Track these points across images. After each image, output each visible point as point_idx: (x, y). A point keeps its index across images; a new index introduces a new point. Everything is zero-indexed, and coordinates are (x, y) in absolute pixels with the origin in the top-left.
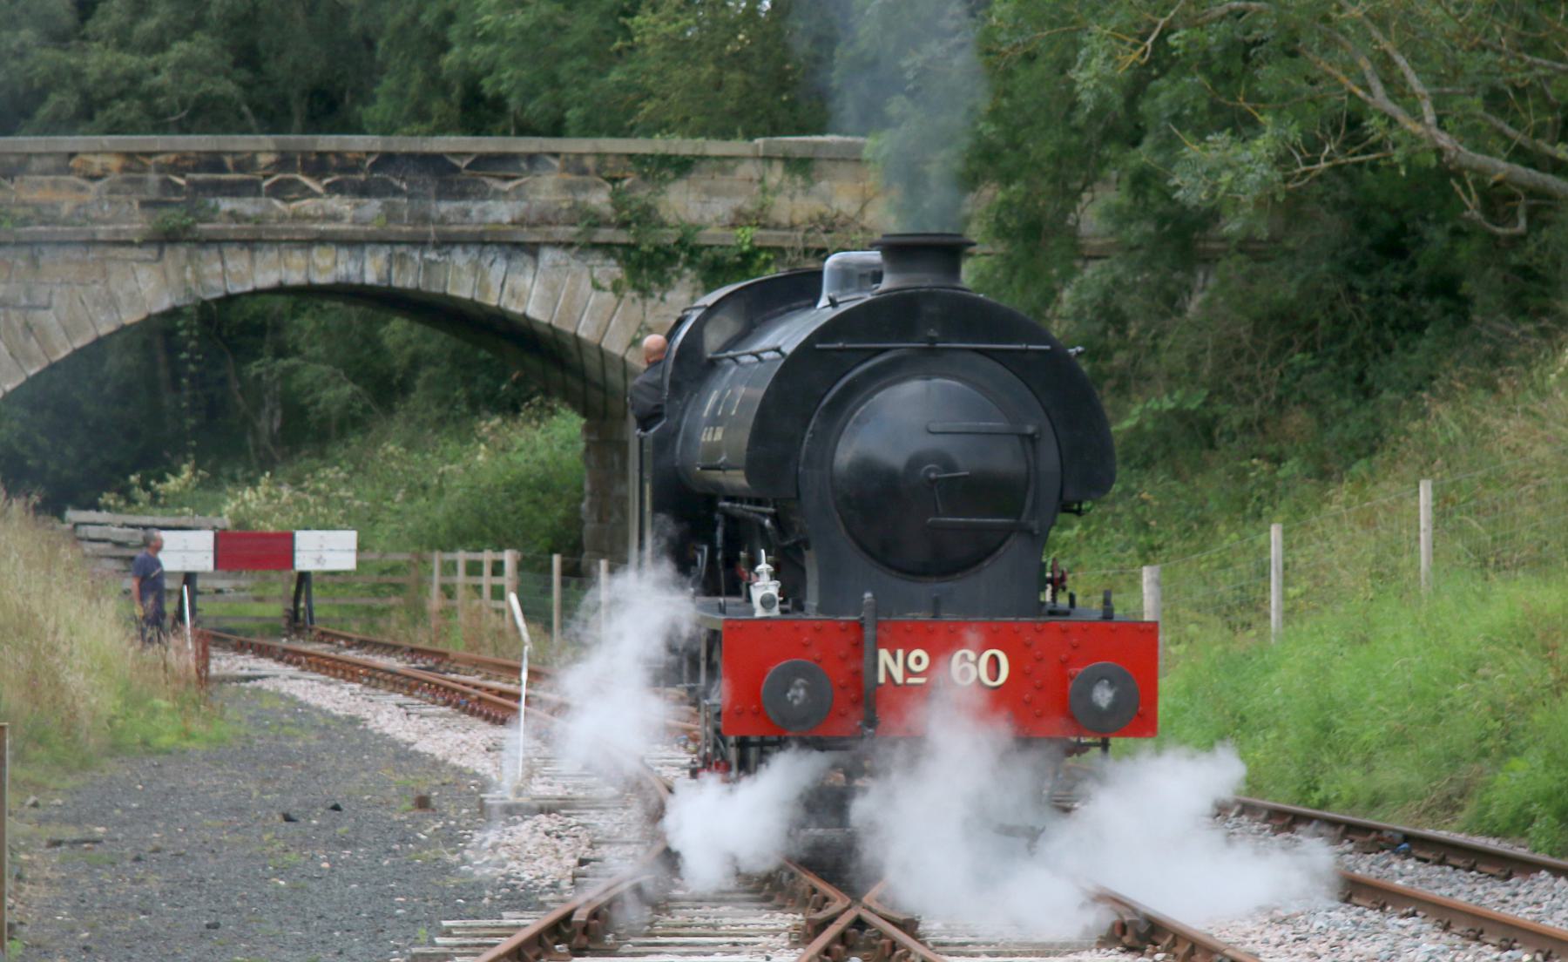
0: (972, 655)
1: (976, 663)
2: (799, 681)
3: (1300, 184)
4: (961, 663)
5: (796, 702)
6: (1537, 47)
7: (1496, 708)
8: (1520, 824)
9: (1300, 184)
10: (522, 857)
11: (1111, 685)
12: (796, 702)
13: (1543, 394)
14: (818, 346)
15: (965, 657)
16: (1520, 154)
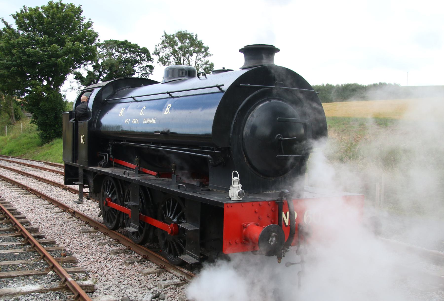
5: (272, 243)
12: (272, 243)
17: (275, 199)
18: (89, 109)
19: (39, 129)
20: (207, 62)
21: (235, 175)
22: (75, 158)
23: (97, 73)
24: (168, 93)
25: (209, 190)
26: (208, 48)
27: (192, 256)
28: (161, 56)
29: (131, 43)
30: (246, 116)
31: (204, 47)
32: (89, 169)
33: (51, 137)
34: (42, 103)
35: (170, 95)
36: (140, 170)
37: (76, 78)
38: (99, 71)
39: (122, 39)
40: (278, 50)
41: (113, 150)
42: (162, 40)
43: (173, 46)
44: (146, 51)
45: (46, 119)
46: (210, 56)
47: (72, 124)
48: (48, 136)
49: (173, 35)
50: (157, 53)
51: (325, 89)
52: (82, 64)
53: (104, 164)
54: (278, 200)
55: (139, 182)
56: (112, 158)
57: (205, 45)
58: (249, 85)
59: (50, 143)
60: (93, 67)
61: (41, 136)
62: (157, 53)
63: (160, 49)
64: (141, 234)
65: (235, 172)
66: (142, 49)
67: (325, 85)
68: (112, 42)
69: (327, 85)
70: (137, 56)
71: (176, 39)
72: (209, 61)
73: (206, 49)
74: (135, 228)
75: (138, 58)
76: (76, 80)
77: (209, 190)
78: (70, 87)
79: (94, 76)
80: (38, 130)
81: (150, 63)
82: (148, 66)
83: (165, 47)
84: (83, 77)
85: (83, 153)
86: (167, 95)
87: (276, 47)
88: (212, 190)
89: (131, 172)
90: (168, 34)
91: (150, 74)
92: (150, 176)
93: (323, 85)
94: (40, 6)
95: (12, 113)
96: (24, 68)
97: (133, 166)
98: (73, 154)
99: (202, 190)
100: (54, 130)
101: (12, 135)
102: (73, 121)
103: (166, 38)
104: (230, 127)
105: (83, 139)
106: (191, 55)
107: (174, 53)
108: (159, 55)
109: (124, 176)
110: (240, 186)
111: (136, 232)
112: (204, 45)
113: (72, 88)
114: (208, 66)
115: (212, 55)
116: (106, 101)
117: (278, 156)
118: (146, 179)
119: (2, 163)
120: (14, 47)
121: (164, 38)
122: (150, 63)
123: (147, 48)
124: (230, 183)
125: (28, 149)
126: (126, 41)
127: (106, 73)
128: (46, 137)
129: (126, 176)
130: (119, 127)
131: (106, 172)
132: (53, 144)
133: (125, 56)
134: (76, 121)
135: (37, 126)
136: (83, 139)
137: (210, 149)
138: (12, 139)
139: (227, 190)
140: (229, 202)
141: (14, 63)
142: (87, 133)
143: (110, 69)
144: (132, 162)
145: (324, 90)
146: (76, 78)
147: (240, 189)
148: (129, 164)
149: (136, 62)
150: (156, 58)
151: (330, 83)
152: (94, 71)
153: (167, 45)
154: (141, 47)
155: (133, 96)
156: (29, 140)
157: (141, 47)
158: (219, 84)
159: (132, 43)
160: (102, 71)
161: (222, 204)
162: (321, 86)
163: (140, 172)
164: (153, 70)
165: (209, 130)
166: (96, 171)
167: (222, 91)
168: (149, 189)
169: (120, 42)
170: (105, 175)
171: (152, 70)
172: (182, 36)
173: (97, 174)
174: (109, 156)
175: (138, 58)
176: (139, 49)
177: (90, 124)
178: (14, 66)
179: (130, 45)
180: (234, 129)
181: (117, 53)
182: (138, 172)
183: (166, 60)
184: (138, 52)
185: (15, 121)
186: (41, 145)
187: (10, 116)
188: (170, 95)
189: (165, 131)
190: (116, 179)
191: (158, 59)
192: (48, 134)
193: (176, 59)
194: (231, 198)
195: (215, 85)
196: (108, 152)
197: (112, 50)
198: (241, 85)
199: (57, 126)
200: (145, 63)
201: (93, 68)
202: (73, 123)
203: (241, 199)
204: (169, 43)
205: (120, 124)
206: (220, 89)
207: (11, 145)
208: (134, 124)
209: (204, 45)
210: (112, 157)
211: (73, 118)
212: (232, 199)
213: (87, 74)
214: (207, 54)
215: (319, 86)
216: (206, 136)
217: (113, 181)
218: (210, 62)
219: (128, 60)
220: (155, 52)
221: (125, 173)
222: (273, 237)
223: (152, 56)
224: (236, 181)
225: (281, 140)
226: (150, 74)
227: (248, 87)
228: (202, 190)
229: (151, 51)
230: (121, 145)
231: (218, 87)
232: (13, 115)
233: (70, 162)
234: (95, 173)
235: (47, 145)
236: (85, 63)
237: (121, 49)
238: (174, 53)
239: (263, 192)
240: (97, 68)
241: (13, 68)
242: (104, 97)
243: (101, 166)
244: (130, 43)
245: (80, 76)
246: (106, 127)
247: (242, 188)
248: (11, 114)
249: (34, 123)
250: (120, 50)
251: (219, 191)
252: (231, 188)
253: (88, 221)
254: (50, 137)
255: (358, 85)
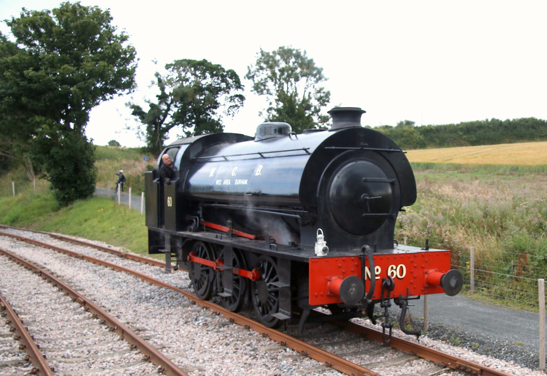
0: (394, 267)
1: (396, 270)
2: (353, 285)
3: (157, 142)
4: (391, 270)
5: (352, 293)
6: (4, 141)
7: (3, 211)
8: (6, 223)
9: (157, 142)
10: (88, 345)
11: (455, 278)
12: (352, 293)
13: (7, 178)
14: (326, 148)
15: (392, 268)
16: (3, 152)
17: (359, 255)
18: (176, 168)
19: (53, 187)
20: (321, 89)
21: (320, 233)
22: (161, 222)
23: (164, 107)
24: (260, 154)
25: (300, 249)
26: (322, 69)
27: (284, 313)
28: (256, 82)
29: (211, 64)
30: (331, 177)
31: (316, 68)
32: (177, 235)
33: (72, 198)
34: (53, 150)
35: (262, 156)
36: (233, 233)
37: (134, 113)
38: (166, 104)
39: (199, 59)
40: (365, 112)
41: (203, 213)
42: (257, 59)
43: (271, 67)
44: (233, 75)
45: (61, 172)
46: (326, 80)
47: (156, 185)
48: (66, 196)
49: (274, 52)
50: (250, 76)
51: (490, 126)
52: (115, 93)
53: (194, 228)
54: (361, 256)
55: (231, 244)
56: (202, 221)
57: (317, 65)
58: (334, 147)
59: (70, 206)
60: (158, 98)
61: (57, 197)
62: (250, 76)
63: (255, 71)
64: (235, 300)
65: (319, 230)
66: (228, 72)
67: (490, 120)
68: (184, 62)
69: (493, 120)
70: (222, 81)
71: (278, 57)
72: (323, 88)
73: (319, 72)
74: (229, 293)
75: (223, 85)
76: (134, 117)
77: (300, 249)
78: (125, 127)
79: (160, 111)
80: (52, 188)
81: (239, 92)
82: (237, 96)
83: (262, 68)
84: (144, 113)
85: (171, 217)
86: (259, 156)
87: (362, 109)
88: (303, 249)
89: (224, 236)
90: (266, 50)
91: (241, 107)
92: (243, 239)
93: (487, 120)
94: (51, 10)
95: (28, 164)
96: (23, 99)
97: (226, 229)
98: (158, 219)
99: (293, 249)
100: (76, 188)
101: (20, 195)
102: (158, 181)
103: (263, 55)
104: (316, 188)
105: (170, 202)
106: (297, 80)
107: (273, 76)
108: (254, 80)
109: (216, 239)
110: (325, 242)
111: (229, 297)
112: (315, 66)
113: (129, 128)
114: (322, 95)
115: (328, 79)
116: (195, 160)
117: (365, 215)
118: (239, 242)
119: (4, 244)
120: (8, 68)
121: (260, 55)
122: (239, 92)
123: (235, 71)
124: (316, 240)
125: (40, 215)
126: (205, 61)
127: (176, 106)
128: (64, 197)
129: (219, 240)
130: (211, 187)
131: (197, 237)
132: (71, 209)
133: (203, 82)
134: (161, 181)
135: (50, 183)
136: (170, 202)
137: (297, 209)
138: (19, 201)
139: (313, 248)
140: (313, 257)
141: (10, 91)
142: (174, 195)
143: (182, 100)
144: (224, 224)
145: (488, 127)
146: (134, 113)
147: (325, 246)
148: (219, 227)
149: (220, 89)
150: (247, 84)
151: (496, 118)
152: (160, 103)
153: (265, 66)
154: (226, 70)
155: (224, 155)
156: (43, 202)
157: (226, 70)
158: (306, 147)
159: (213, 64)
160: (172, 103)
161: (307, 259)
162: (484, 122)
163: (233, 236)
164: (244, 101)
165: (296, 190)
166: (185, 236)
167: (309, 154)
168: (242, 251)
169: (197, 62)
170: (195, 240)
171: (243, 101)
172: (286, 53)
173: (187, 240)
174: (200, 219)
175: (223, 85)
176: (224, 71)
177: (178, 185)
178: (9, 95)
179: (210, 66)
180: (320, 190)
181: (193, 78)
182: (230, 236)
183: (262, 87)
184: (223, 76)
185: (34, 176)
186: (56, 210)
187: (26, 168)
188: (262, 156)
189: (257, 192)
190: (208, 244)
191: (253, 85)
192: (67, 194)
193: (277, 86)
194: (316, 255)
195: (302, 148)
196: (199, 215)
197: (186, 73)
198: (326, 148)
199: (79, 182)
200: (233, 92)
201: (159, 99)
202: (158, 184)
203: (326, 255)
204: (267, 63)
205: (211, 184)
206: (307, 152)
207: (17, 210)
208: (226, 185)
209: (315, 66)
210: (202, 220)
211: (158, 177)
212: (318, 255)
213: (149, 108)
214: (320, 79)
215: (481, 122)
216: (293, 196)
217: (204, 245)
218: (325, 90)
219: (209, 88)
220: (247, 76)
221: (217, 237)
222: (352, 288)
223: (243, 81)
224: (321, 238)
225: (366, 200)
226: (241, 107)
227: (332, 149)
228: (293, 249)
229: (241, 74)
230: (213, 207)
231: (305, 150)
232: (31, 166)
233: (155, 228)
234: (184, 238)
235: (64, 209)
236: (120, 91)
237: (200, 73)
238: (273, 76)
239: (351, 250)
240: (163, 100)
241: (6, 99)
242: (192, 156)
243: (190, 231)
244: (210, 63)
245: (138, 111)
246: (196, 188)
247: (326, 245)
248: (27, 166)
249: (45, 179)
250: (198, 73)
251: (308, 249)
252: (316, 244)
253: (178, 290)
254: (69, 198)
255: (536, 119)
